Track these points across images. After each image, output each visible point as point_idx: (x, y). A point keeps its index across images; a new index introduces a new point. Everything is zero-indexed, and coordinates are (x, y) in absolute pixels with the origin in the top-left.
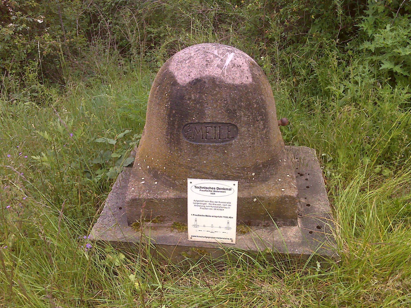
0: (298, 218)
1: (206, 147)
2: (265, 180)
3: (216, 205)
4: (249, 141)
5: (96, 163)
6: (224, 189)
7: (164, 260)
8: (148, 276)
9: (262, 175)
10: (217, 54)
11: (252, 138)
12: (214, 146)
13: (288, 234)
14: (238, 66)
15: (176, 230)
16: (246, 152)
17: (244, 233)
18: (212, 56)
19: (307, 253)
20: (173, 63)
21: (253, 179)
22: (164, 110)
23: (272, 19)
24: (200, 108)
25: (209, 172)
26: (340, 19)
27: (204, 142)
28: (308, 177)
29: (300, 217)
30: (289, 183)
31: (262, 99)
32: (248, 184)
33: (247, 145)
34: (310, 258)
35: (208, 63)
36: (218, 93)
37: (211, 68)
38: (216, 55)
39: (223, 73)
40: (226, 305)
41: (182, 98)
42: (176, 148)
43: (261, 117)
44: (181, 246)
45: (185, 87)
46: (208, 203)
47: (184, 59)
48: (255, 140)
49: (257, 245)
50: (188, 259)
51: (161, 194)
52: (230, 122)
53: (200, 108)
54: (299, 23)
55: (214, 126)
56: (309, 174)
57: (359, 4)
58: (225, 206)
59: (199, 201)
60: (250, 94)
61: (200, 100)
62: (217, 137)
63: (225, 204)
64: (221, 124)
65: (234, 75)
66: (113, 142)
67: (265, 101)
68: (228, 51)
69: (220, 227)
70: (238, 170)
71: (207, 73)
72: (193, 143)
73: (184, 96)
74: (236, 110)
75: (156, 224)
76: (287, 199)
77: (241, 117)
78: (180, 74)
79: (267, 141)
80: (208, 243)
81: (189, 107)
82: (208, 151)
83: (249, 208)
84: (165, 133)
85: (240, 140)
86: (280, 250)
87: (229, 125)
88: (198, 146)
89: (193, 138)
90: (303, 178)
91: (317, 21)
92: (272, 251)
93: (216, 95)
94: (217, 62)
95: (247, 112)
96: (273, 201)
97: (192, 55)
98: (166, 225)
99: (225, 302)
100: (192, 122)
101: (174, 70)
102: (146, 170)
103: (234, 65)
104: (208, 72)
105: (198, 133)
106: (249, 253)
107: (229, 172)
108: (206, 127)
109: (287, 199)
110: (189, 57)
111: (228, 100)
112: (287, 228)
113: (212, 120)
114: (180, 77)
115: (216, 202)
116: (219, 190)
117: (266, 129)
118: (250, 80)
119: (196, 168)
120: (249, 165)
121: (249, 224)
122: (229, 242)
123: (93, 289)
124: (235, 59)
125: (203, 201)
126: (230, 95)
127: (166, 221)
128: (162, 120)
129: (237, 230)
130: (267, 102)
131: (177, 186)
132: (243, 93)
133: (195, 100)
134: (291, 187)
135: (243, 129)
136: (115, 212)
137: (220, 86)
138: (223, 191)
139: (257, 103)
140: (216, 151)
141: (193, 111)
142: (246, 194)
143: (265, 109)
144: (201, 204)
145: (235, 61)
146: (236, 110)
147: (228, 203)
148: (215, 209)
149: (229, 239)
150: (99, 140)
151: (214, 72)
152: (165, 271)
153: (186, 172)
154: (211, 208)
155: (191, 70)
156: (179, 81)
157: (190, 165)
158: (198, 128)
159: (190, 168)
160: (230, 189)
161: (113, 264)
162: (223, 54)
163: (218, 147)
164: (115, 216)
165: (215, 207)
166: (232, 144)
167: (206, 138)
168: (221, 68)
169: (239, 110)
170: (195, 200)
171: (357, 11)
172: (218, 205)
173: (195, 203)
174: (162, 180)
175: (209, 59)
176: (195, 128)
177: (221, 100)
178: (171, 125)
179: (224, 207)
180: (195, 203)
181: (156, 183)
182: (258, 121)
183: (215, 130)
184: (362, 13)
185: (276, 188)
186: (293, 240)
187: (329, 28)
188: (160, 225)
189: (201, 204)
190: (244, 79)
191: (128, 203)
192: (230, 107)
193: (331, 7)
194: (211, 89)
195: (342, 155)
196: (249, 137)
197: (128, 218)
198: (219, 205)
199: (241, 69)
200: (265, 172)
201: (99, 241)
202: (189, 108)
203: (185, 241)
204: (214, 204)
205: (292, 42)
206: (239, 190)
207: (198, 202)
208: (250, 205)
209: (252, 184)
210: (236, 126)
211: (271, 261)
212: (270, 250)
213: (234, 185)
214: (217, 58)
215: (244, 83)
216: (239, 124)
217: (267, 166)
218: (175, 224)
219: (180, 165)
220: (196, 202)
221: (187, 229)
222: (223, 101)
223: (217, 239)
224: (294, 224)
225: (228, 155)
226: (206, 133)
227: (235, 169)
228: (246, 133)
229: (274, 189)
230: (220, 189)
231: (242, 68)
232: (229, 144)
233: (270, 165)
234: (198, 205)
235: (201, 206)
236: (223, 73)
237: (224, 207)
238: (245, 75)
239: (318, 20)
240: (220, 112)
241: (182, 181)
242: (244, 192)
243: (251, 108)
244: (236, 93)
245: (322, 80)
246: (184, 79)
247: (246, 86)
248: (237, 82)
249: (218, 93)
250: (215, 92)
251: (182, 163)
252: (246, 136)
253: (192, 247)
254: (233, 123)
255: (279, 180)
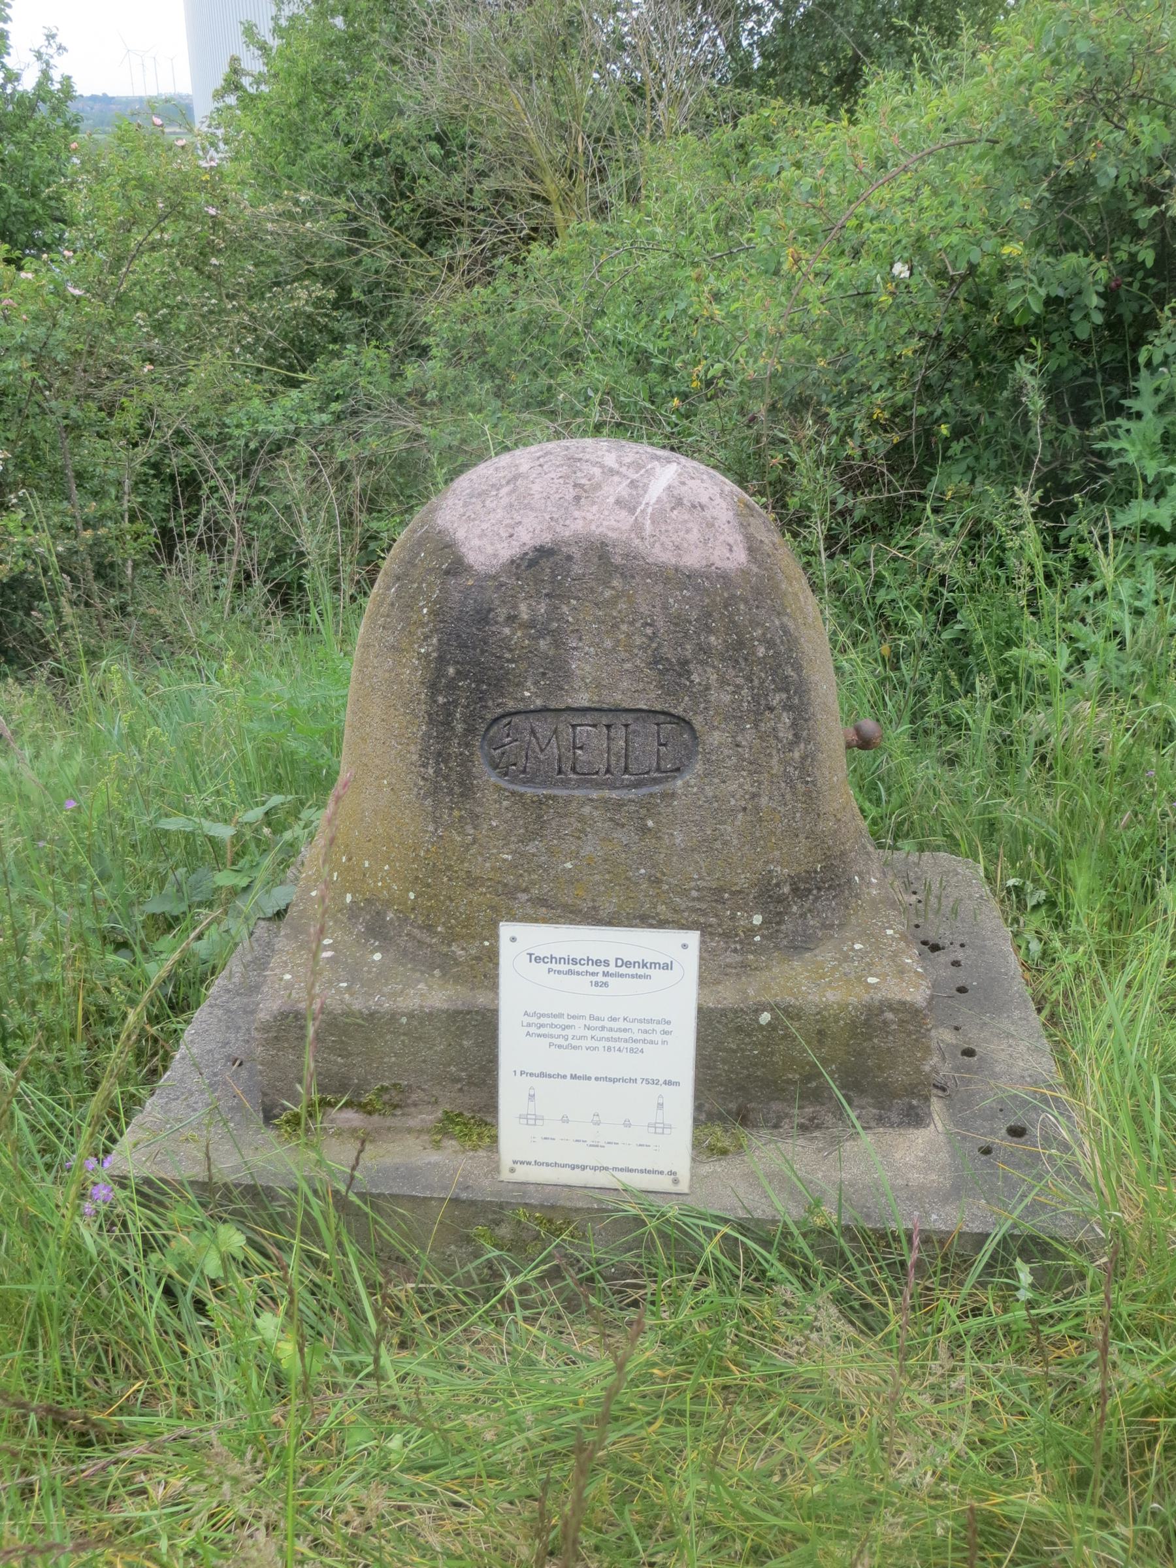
0: (934, 1100)
1: (574, 804)
2: (800, 945)
3: (611, 1030)
4: (741, 786)
5: (158, 910)
6: (644, 965)
7: (404, 1262)
8: (335, 1325)
9: (790, 926)
10: (616, 466)
11: (751, 773)
12: (606, 801)
13: (897, 1156)
14: (694, 507)
15: (454, 1142)
16: (729, 829)
17: (724, 1152)
18: (597, 471)
19: (976, 1227)
20: (450, 502)
21: (757, 938)
22: (416, 669)
23: (799, 444)
24: (551, 653)
25: (584, 906)
26: (1038, 438)
27: (565, 783)
28: (960, 955)
29: (940, 1093)
30: (895, 955)
31: (783, 627)
32: (738, 958)
33: (733, 802)
34: (989, 1247)
35: (582, 494)
36: (617, 597)
37: (595, 509)
38: (611, 470)
39: (638, 528)
40: (654, 1437)
41: (483, 616)
42: (456, 813)
43: (784, 696)
44: (473, 1203)
45: (494, 578)
46: (579, 1023)
47: (493, 486)
48: (760, 783)
49: (775, 1199)
50: (497, 1253)
51: (393, 995)
52: (665, 707)
53: (551, 653)
54: (898, 452)
55: (605, 721)
56: (962, 945)
57: (1104, 384)
58: (648, 1037)
59: (543, 1015)
60: (742, 607)
61: (550, 620)
62: (618, 764)
63: (649, 1027)
64: (632, 715)
65: (681, 534)
66: (224, 832)
67: (796, 640)
68: (658, 458)
69: (627, 1124)
70: (698, 899)
71: (578, 526)
72: (521, 789)
73: (490, 610)
74: (687, 662)
75: (376, 1118)
76: (889, 1016)
77: (708, 688)
78: (478, 531)
79: (807, 794)
80: (580, 1192)
81: (511, 650)
82: (581, 819)
83: (743, 1050)
84: (415, 757)
85: (706, 780)
86: (868, 1217)
87: (662, 718)
88: (540, 802)
89: (524, 772)
90: (942, 958)
91: (956, 447)
92: (835, 1217)
93: (613, 602)
94: (618, 488)
95: (731, 671)
96: (836, 1022)
97: (524, 468)
98: (412, 1123)
99: (650, 1424)
100: (521, 706)
101: (452, 522)
102: (340, 911)
103: (679, 502)
104: (580, 523)
105: (542, 750)
106: (742, 1227)
107: (662, 908)
108: (574, 726)
109: (889, 1016)
110: (510, 476)
111: (660, 623)
112: (890, 1136)
113: (596, 698)
114: (476, 542)
115: (614, 1019)
116: (624, 970)
117: (802, 746)
118: (741, 556)
119: (535, 891)
120: (742, 880)
121: (744, 1118)
122: (664, 1183)
123: (109, 1372)
124: (684, 483)
125: (561, 1016)
126: (665, 607)
127: (415, 1105)
128: (406, 705)
129: (697, 1144)
130: (807, 647)
131: (457, 963)
132: (713, 601)
133: (532, 624)
134: (902, 972)
135: (716, 738)
136: (215, 1075)
137: (626, 573)
138: (641, 971)
139: (770, 644)
140: (611, 819)
141: (523, 665)
142: (728, 996)
143: (798, 668)
144: (551, 1026)
145: (684, 489)
146: (687, 662)
147: (659, 1022)
148: (609, 1049)
149: (661, 1173)
150: (175, 824)
151: (605, 523)
152: (404, 1307)
153: (492, 908)
154: (594, 1044)
155: (518, 519)
156: (471, 558)
157: (510, 879)
158: (543, 728)
159: (511, 892)
160: (667, 967)
161: (197, 1270)
162: (638, 466)
163: (620, 804)
164: (215, 1090)
165: (608, 1039)
166: (673, 795)
167: (574, 770)
168: (632, 510)
169: (702, 663)
170: (530, 1011)
171: (1097, 410)
172: (619, 1030)
173: (529, 1025)
174: (402, 944)
175: (583, 481)
176: (533, 732)
177: (632, 623)
178: (441, 720)
179: (644, 1041)
180: (529, 1025)
181: (377, 957)
182: (771, 709)
183: (609, 738)
184: (1116, 410)
185: (845, 974)
186: (916, 1178)
187: (1001, 467)
188: (389, 1121)
189: (551, 1026)
190: (717, 553)
191: (265, 1028)
192: (667, 651)
193: (1005, 394)
194: (594, 584)
195: (1082, 878)
196: (737, 768)
197: (265, 1094)
198: (625, 1030)
199: (704, 518)
200: (803, 916)
201: (148, 1181)
202: (508, 656)
203: (486, 1182)
204: (603, 1028)
205: (866, 529)
206: (703, 982)
207: (543, 1020)
208: (747, 1040)
209: (751, 957)
210: (688, 723)
211: (836, 1259)
212: (828, 1216)
213: (685, 946)
214: (616, 479)
215: (719, 564)
216: (700, 718)
217: (810, 891)
218: (449, 1118)
219: (472, 882)
220: (534, 1020)
221: (495, 1139)
222: (638, 625)
223: (618, 1174)
224: (915, 1118)
225: (659, 838)
226: (575, 748)
227: (685, 893)
228: (726, 752)
229: (840, 979)
230: (627, 964)
231: (707, 514)
232: (664, 796)
233: (819, 889)
234: (542, 1031)
235: (552, 1036)
236: (638, 528)
237: (644, 1041)
238: (722, 538)
239: (962, 444)
240: (627, 666)
241: (477, 943)
242: (720, 988)
243: (746, 660)
244: (686, 600)
245: (987, 639)
246: (490, 550)
247: (724, 577)
248: (692, 560)
249: (617, 597)
250: (608, 594)
251: (477, 872)
252: (729, 763)
253: (514, 1206)
254: (679, 711)
255: (857, 946)
